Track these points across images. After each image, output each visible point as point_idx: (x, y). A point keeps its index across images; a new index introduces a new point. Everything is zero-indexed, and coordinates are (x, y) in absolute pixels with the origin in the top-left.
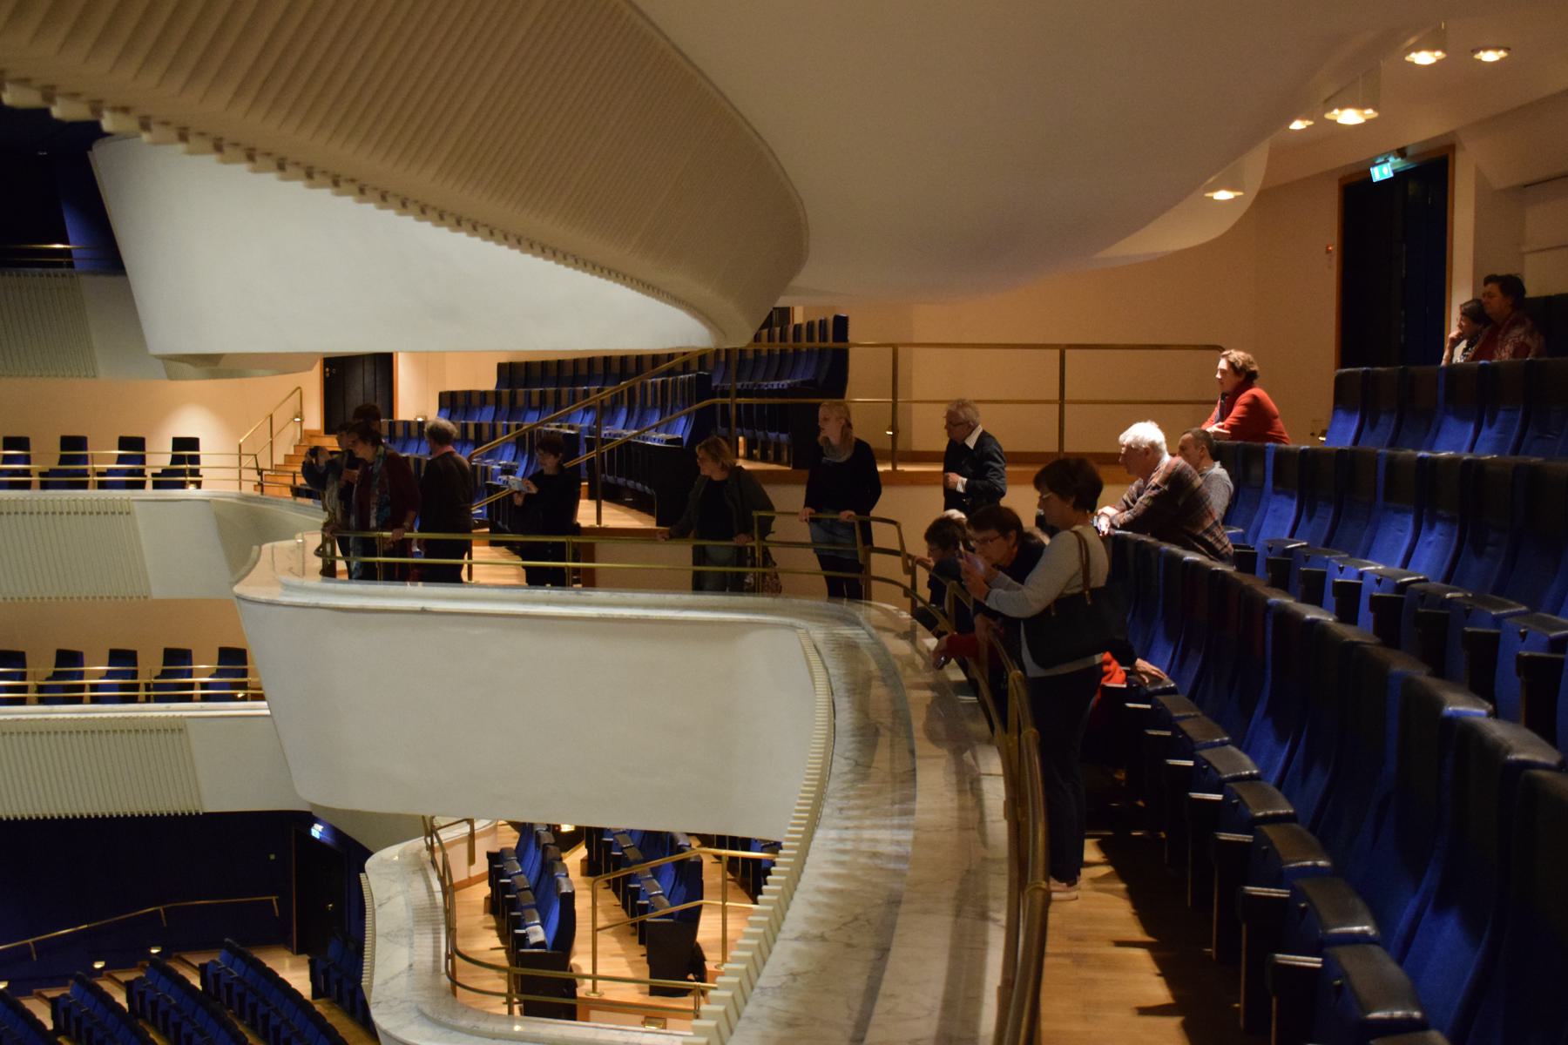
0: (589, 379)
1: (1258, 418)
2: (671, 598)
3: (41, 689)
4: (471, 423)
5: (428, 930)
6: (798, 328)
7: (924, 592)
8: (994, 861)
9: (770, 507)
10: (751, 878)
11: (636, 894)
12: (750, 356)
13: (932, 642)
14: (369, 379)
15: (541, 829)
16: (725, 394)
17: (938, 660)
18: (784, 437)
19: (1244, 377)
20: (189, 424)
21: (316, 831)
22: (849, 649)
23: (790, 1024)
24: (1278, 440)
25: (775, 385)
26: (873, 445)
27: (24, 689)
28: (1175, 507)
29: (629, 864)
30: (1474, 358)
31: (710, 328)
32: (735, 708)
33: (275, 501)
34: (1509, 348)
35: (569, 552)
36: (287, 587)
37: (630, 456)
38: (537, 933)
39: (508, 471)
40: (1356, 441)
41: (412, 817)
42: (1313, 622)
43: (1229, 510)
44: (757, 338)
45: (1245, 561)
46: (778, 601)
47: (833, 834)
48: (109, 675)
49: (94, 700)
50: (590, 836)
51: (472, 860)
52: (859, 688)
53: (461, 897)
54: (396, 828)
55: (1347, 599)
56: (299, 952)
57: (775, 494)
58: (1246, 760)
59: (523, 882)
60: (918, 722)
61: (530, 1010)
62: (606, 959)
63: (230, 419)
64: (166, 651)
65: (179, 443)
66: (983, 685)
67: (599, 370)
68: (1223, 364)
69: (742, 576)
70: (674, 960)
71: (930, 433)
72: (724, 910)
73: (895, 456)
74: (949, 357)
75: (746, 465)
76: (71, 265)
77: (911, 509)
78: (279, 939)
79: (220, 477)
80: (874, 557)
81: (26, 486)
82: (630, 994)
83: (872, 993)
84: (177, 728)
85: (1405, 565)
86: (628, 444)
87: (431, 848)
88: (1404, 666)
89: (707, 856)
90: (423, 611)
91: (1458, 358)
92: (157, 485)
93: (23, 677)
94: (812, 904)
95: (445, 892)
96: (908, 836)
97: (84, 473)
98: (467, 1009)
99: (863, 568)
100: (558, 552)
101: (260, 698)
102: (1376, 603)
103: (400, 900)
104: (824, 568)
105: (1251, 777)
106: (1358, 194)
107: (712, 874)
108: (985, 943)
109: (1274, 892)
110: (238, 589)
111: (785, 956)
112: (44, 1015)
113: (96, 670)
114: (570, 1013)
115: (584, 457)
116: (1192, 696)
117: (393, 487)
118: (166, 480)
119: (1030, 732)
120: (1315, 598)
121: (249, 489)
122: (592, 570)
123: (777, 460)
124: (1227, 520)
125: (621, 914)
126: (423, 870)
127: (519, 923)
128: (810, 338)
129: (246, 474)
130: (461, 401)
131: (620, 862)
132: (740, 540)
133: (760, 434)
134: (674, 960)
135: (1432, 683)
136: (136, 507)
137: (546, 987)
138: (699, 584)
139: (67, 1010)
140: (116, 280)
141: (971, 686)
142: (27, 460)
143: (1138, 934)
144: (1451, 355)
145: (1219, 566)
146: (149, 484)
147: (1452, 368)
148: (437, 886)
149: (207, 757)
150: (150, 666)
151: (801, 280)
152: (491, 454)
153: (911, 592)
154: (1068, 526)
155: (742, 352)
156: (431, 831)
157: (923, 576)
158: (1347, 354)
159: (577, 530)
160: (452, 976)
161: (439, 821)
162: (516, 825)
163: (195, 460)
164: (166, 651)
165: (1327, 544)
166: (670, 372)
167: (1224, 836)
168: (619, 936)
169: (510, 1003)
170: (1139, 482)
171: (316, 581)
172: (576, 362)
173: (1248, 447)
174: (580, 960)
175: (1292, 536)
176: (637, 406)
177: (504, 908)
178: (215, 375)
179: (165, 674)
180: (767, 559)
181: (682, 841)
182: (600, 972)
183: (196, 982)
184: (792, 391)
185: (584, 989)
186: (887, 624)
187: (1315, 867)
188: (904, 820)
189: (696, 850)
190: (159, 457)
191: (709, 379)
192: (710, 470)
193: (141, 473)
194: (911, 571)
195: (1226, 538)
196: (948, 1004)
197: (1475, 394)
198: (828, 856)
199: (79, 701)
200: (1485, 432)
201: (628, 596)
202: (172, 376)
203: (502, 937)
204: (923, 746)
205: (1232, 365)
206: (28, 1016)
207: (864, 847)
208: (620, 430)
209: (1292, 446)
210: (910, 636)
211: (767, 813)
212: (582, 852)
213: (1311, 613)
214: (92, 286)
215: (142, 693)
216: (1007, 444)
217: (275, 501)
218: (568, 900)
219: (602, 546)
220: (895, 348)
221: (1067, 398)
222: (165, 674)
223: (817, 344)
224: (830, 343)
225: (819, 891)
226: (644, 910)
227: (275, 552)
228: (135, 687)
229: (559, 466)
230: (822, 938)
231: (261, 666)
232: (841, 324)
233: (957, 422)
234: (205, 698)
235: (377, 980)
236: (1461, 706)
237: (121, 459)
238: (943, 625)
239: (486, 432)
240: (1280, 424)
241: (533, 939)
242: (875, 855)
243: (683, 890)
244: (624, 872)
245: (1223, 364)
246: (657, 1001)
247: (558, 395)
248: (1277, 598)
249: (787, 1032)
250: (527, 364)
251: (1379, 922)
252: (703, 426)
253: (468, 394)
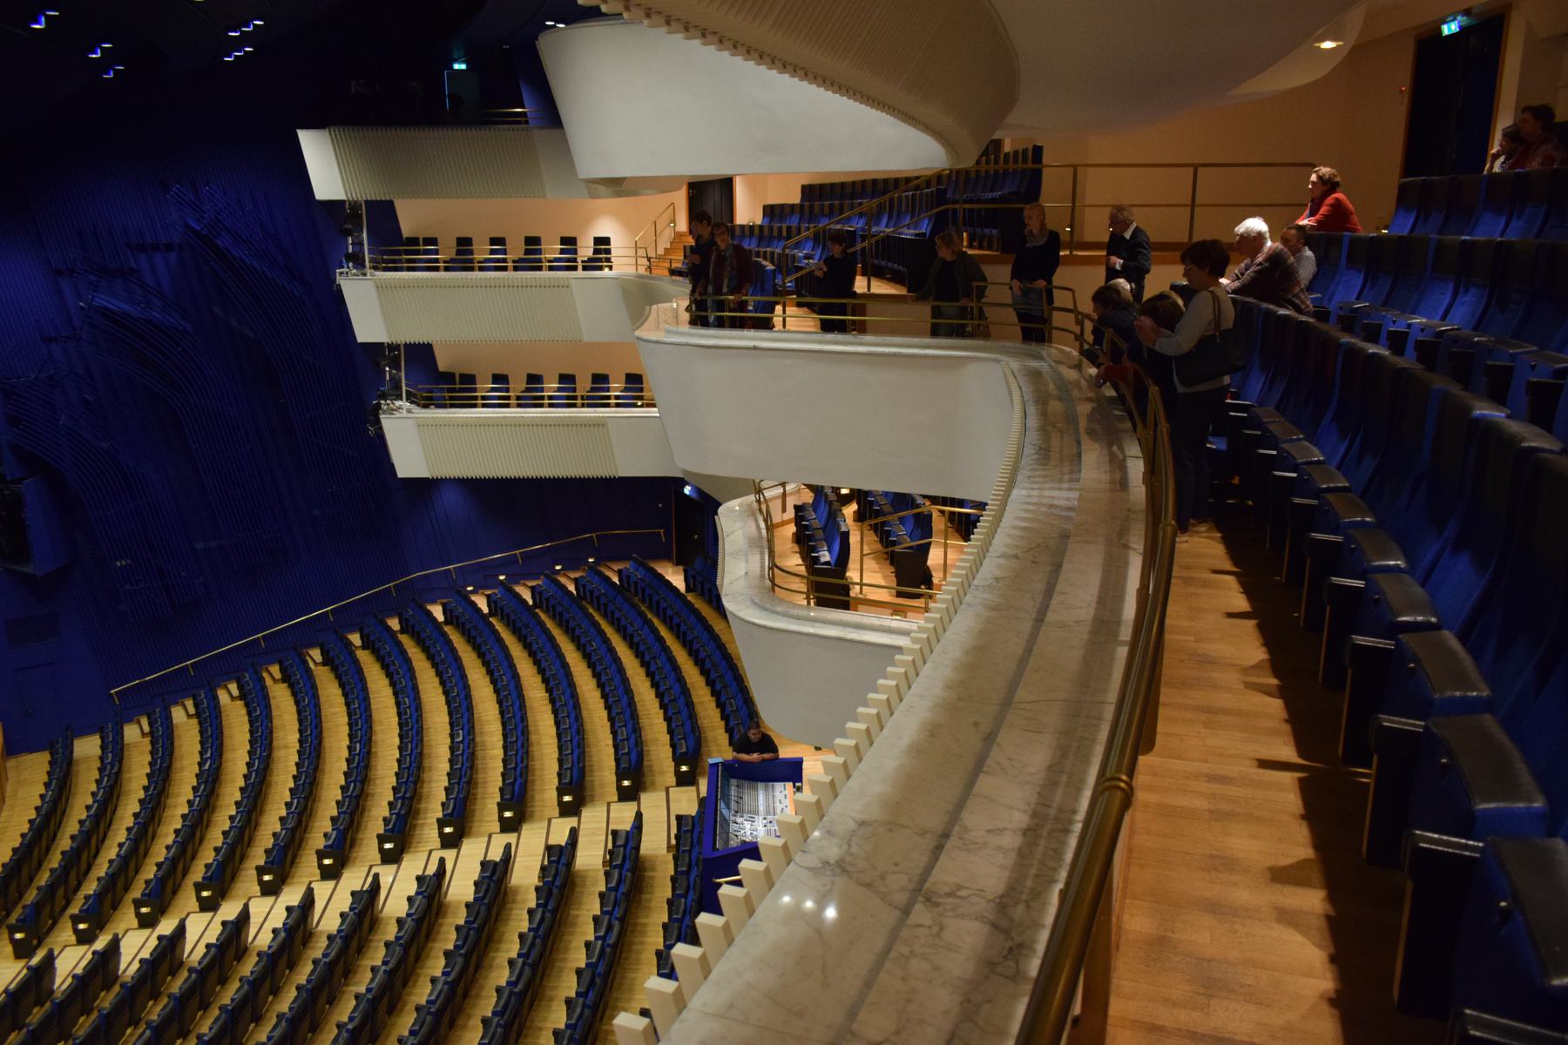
0: (862, 195)
1: (1339, 216)
2: (916, 340)
3: (518, 398)
4: (784, 226)
5: (757, 551)
6: (1007, 155)
7: (1089, 337)
8: (1135, 512)
9: (984, 279)
10: (964, 527)
11: (889, 533)
12: (973, 175)
13: (1093, 371)
14: (717, 197)
15: (828, 491)
16: (955, 202)
17: (1097, 383)
18: (995, 232)
19: (1329, 185)
20: (604, 228)
21: (687, 490)
22: (1035, 375)
23: (995, 608)
24: (1355, 230)
25: (990, 195)
27: (508, 398)
28: (1273, 278)
29: (884, 514)
30: (1512, 167)
31: (948, 151)
32: (960, 413)
33: (659, 278)
34: (1539, 159)
35: (849, 310)
36: (669, 332)
37: (890, 246)
38: (825, 556)
39: (808, 257)
40: (1412, 231)
41: (746, 480)
42: (1374, 354)
43: (1312, 282)
44: (978, 162)
45: (1322, 315)
46: (988, 343)
47: (1024, 492)
48: (559, 390)
49: (551, 406)
50: (858, 495)
51: (784, 510)
52: (1042, 399)
53: (778, 533)
54: (737, 487)
55: (1397, 342)
56: (677, 564)
57: (988, 270)
58: (1315, 450)
59: (817, 524)
60: (1083, 424)
61: (821, 603)
62: (868, 573)
63: (629, 225)
66: (1129, 398)
67: (869, 189)
68: (1314, 177)
69: (963, 326)
70: (912, 577)
71: (1097, 228)
72: (946, 546)
73: (1072, 245)
74: (1112, 172)
75: (970, 252)
76: (527, 122)
77: (1078, 282)
78: (665, 556)
79: (623, 263)
80: (1055, 313)
81: (505, 269)
82: (884, 596)
83: (1049, 592)
84: (601, 424)
85: (1443, 318)
86: (888, 237)
87: (759, 501)
88: (1441, 383)
89: (935, 511)
90: (755, 348)
91: (1497, 169)
92: (585, 268)
93: (507, 390)
94: (1014, 528)
95: (768, 529)
96: (1076, 495)
97: (540, 261)
98: (782, 600)
99: (1047, 321)
100: (842, 310)
101: (653, 406)
102: (1419, 345)
103: (740, 533)
104: (1020, 321)
105: (1319, 462)
106: (1429, 44)
107: (938, 523)
108: (1127, 563)
109: (1332, 538)
110: (637, 333)
111: (991, 568)
112: (527, 596)
113: (551, 386)
114: (845, 606)
115: (859, 247)
116: (1277, 408)
117: (728, 268)
118: (592, 265)
119: (1164, 427)
120: (1374, 340)
121: (642, 270)
122: (864, 322)
123: (990, 248)
124: (1310, 288)
125: (878, 546)
126: (754, 514)
127: (814, 549)
128: (1016, 161)
129: (640, 261)
130: (777, 212)
131: (878, 514)
132: (964, 302)
133: (978, 230)
134: (912, 577)
135: (1462, 394)
137: (831, 590)
138: (935, 332)
139: (540, 594)
140: (555, 132)
141: (1121, 399)
142: (505, 252)
143: (1229, 566)
144: (1492, 167)
145: (1304, 318)
147: (1492, 176)
148: (763, 525)
149: (618, 443)
150: (584, 385)
151: (1011, 119)
152: (797, 245)
153: (1079, 338)
154: (1205, 288)
155: (967, 172)
156: (759, 491)
157: (1089, 326)
158: (1409, 167)
159: (855, 295)
160: (772, 580)
161: (764, 485)
162: (809, 486)
163: (608, 251)
165: (1384, 304)
166: (917, 188)
167: (1297, 500)
168: (877, 560)
169: (808, 599)
170: (1247, 261)
171: (686, 328)
173: (1332, 237)
174: (853, 574)
175: (1358, 298)
176: (895, 212)
177: (805, 540)
178: (619, 195)
179: (593, 390)
180: (981, 315)
181: (920, 501)
183: (616, 580)
184: (1002, 199)
185: (855, 592)
186: (1062, 357)
187: (1364, 522)
188: (1072, 485)
189: (927, 507)
190: (586, 250)
191: (945, 191)
192: (945, 254)
193: (575, 260)
194: (1080, 323)
195: (1309, 301)
196: (1101, 600)
197: (1509, 195)
198: (1020, 505)
199: (541, 406)
200: (1514, 223)
201: (888, 339)
202: (593, 196)
203: (803, 558)
204: (1084, 438)
205: (1320, 178)
206: (518, 596)
207: (1045, 501)
208: (883, 228)
209: (1362, 233)
210: (1078, 367)
211: (977, 480)
212: (854, 507)
213: (1372, 349)
214: (541, 136)
215: (579, 402)
216: (1154, 237)
217: (659, 278)
218: (845, 536)
219: (871, 306)
220: (1075, 167)
221: (1197, 202)
222: (593, 390)
223: (1020, 165)
224: (1030, 165)
225: (1014, 528)
226: (894, 543)
227: (660, 310)
228: (575, 398)
229: (844, 251)
230: (1016, 557)
231: (652, 385)
232: (1038, 151)
233: (1118, 220)
234: (618, 405)
235: (726, 581)
236: (1485, 410)
238: (1102, 359)
239: (794, 231)
240: (1355, 218)
241: (823, 560)
242: (1052, 506)
243: (919, 532)
244: (880, 519)
245: (1314, 177)
246: (900, 601)
247: (841, 206)
248: (1346, 339)
249: (993, 614)
251: (1408, 557)
252: (940, 224)
253: (782, 206)
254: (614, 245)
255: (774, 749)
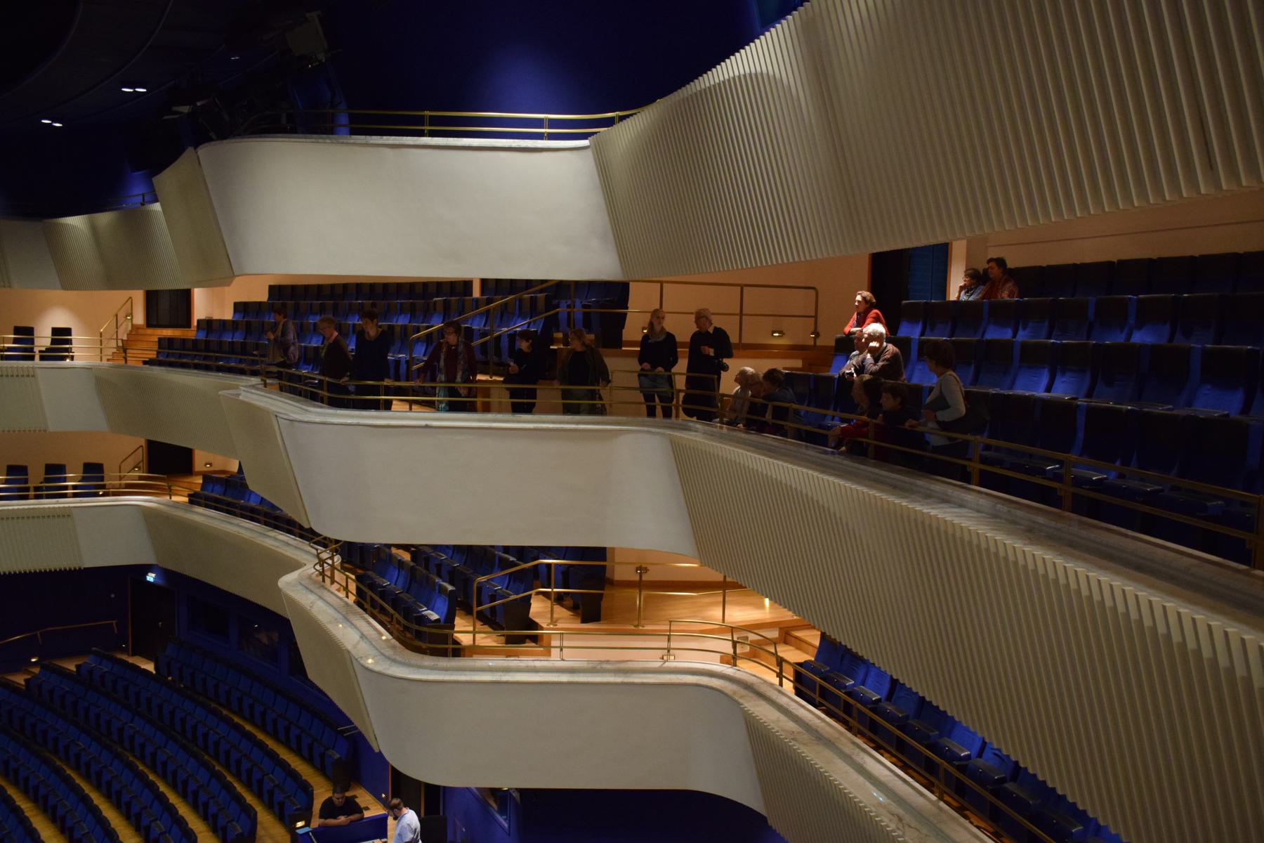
3: (37, 489)
26: (678, 339)
64: (47, 466)
65: (56, 331)
79: (83, 353)
84: (66, 514)
90: (427, 426)
92: (42, 358)
136: (38, 371)
146: (37, 357)
150: (36, 476)
164: (47, 466)
172: (333, 286)
182: (471, 636)
190: (43, 340)
193: (31, 350)
205: (864, 298)
215: (32, 493)
220: (662, 283)
228: (27, 489)
234: (75, 495)
237: (15, 341)
245: (859, 298)
250: (293, 287)
254: (74, 337)
255: (359, 810)
